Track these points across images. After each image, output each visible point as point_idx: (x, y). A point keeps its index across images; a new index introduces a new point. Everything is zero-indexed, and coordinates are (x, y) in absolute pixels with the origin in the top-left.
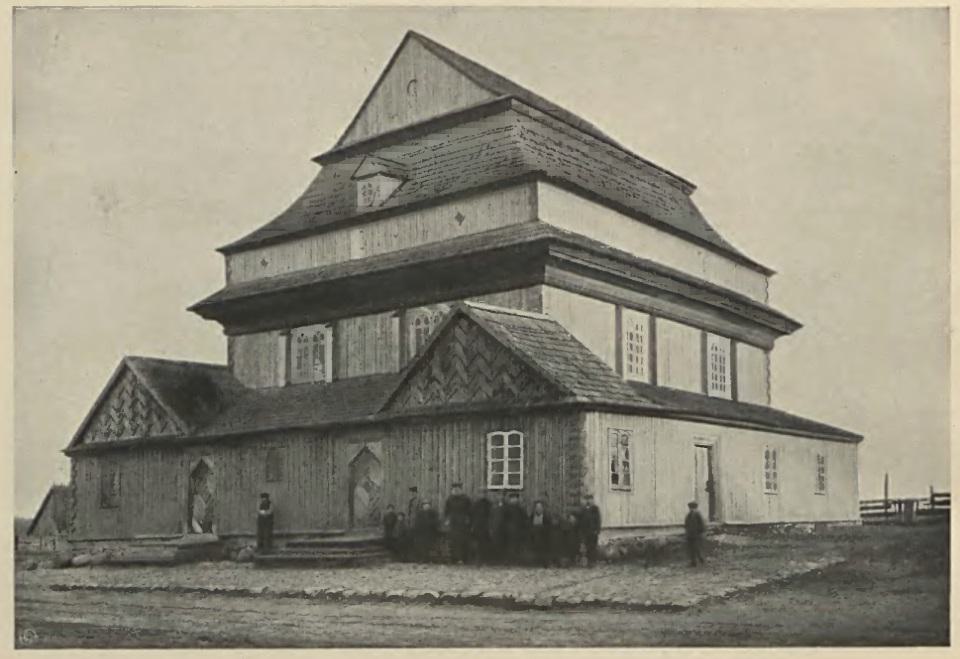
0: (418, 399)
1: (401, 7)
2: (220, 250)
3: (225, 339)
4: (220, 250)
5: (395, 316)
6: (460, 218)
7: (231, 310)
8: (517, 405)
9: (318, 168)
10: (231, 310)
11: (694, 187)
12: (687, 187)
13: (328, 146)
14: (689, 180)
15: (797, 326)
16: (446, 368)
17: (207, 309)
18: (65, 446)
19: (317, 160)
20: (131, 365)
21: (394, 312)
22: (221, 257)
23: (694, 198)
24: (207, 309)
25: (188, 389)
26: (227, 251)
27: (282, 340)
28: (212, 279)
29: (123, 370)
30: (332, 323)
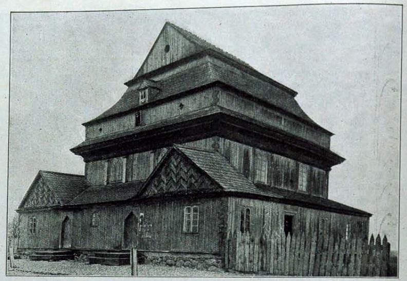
0: (153, 191)
1: (267, 77)
2: (83, 124)
3: (84, 163)
4: (83, 124)
5: (152, 153)
6: (181, 106)
7: (87, 152)
8: (211, 191)
9: (127, 87)
10: (87, 152)
11: (297, 93)
12: (294, 94)
13: (131, 76)
14: (294, 90)
15: (72, 150)
16: (167, 175)
17: (77, 150)
18: (17, 208)
19: (126, 84)
20: (44, 175)
21: (151, 151)
22: (84, 128)
23: (296, 98)
24: (77, 150)
25: (75, 183)
26: (87, 125)
27: (106, 164)
28: (80, 137)
29: (39, 176)
30: (127, 156)
